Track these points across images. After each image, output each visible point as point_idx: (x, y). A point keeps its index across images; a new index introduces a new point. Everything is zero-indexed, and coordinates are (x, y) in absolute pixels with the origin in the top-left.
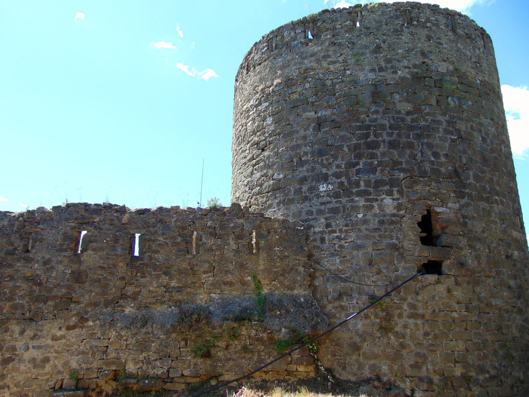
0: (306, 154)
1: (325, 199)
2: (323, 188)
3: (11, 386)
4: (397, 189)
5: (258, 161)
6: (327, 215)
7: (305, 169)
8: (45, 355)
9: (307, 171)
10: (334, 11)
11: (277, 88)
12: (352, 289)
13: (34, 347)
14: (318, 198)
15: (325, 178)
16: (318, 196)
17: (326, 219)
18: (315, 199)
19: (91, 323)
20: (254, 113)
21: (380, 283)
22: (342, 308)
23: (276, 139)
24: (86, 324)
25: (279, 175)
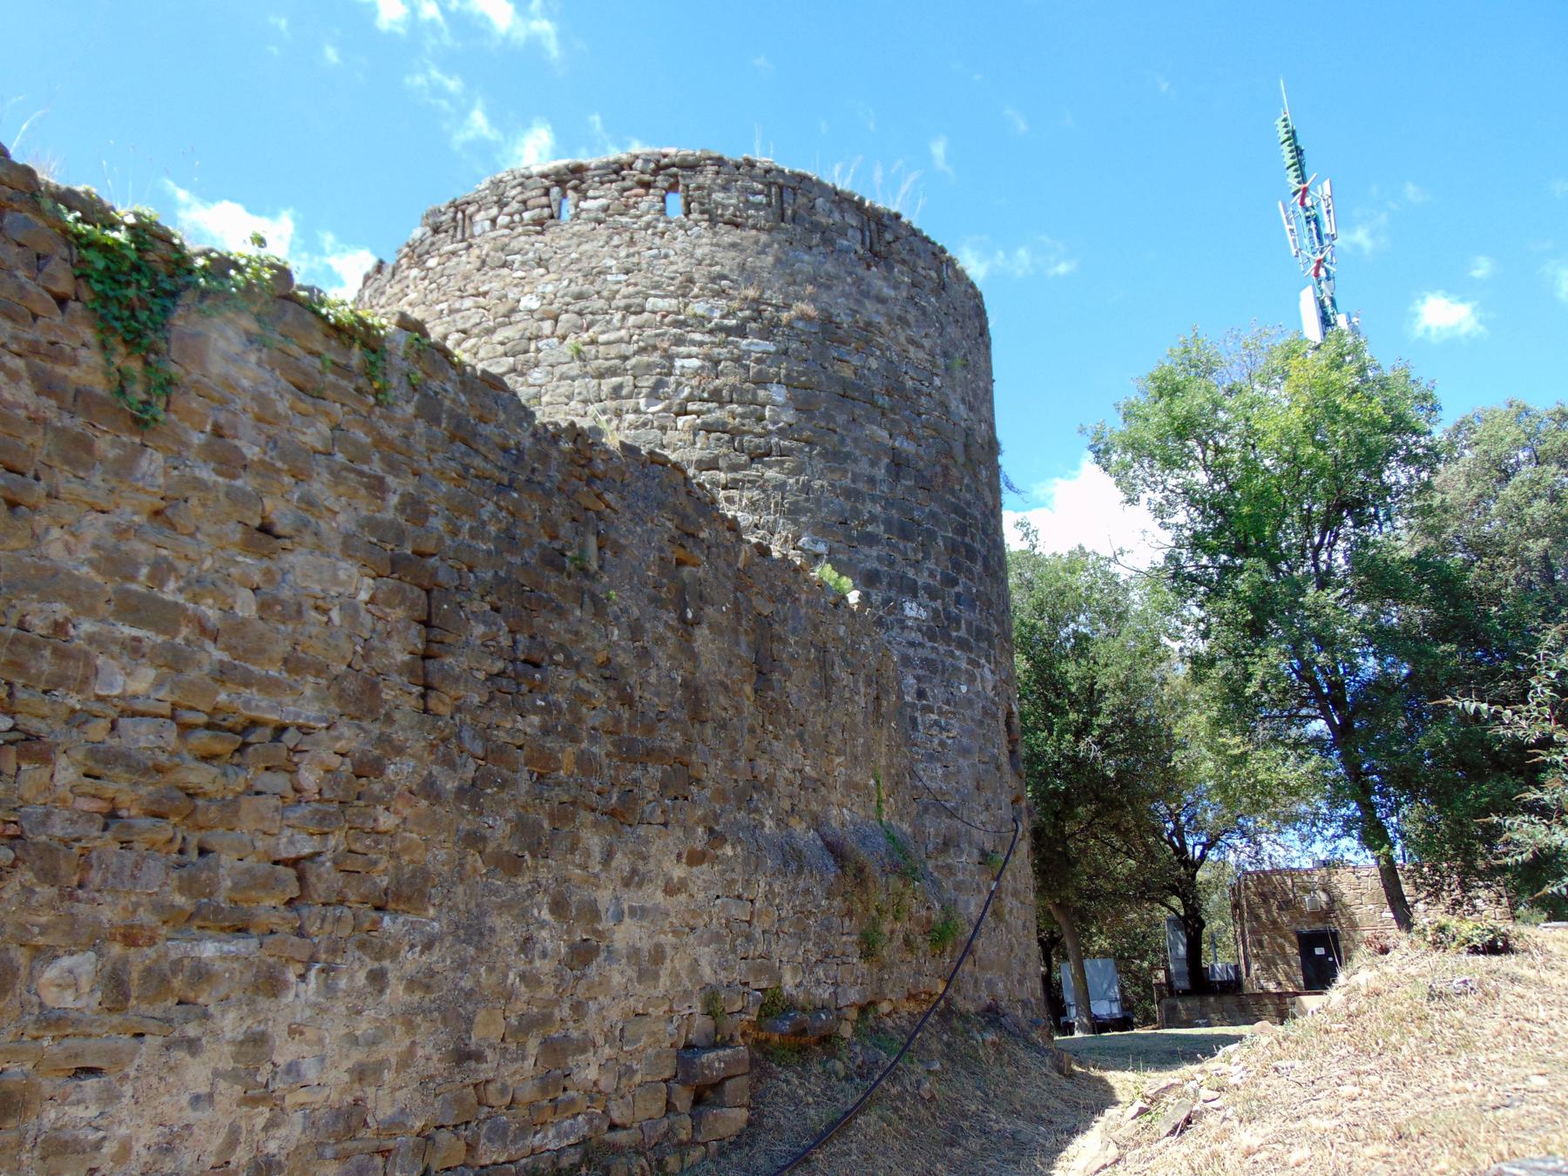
0: (873, 519)
1: (915, 636)
2: (911, 610)
3: (600, 1040)
4: (134, 587)
5: (735, 481)
6: (920, 672)
7: (874, 554)
8: (656, 939)
9: (879, 559)
10: (926, 240)
11: (800, 325)
12: (959, 834)
13: (633, 912)
14: (903, 628)
15: (912, 590)
16: (902, 623)
17: (918, 678)
18: (897, 630)
19: (729, 851)
20: (701, 344)
21: (989, 827)
22: (949, 867)
23: (801, 450)
24: (719, 852)
25: (815, 542)
